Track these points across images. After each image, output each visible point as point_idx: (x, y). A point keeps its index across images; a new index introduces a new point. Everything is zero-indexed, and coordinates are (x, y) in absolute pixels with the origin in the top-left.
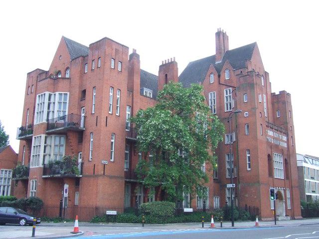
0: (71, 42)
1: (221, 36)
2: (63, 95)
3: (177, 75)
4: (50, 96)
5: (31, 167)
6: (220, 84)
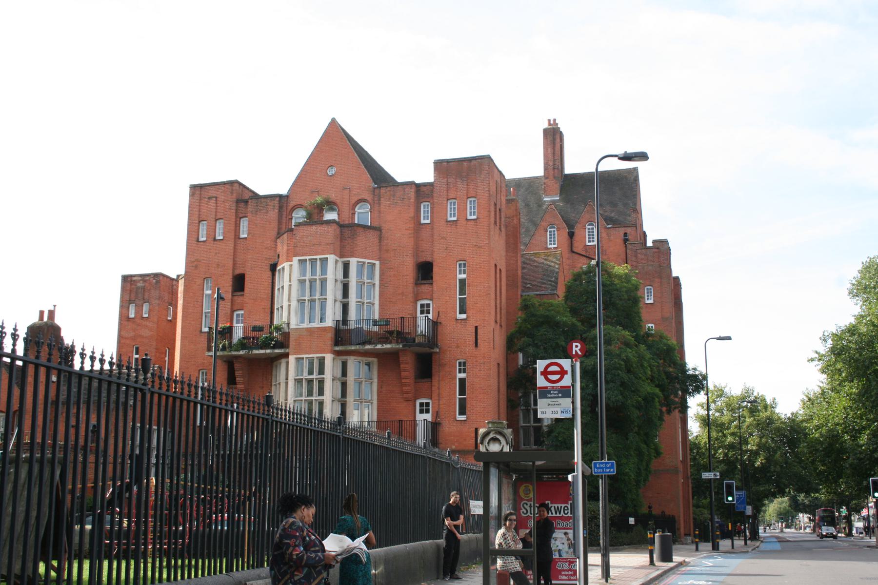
0: (637, 176)
1: (553, 137)
6: (379, 229)
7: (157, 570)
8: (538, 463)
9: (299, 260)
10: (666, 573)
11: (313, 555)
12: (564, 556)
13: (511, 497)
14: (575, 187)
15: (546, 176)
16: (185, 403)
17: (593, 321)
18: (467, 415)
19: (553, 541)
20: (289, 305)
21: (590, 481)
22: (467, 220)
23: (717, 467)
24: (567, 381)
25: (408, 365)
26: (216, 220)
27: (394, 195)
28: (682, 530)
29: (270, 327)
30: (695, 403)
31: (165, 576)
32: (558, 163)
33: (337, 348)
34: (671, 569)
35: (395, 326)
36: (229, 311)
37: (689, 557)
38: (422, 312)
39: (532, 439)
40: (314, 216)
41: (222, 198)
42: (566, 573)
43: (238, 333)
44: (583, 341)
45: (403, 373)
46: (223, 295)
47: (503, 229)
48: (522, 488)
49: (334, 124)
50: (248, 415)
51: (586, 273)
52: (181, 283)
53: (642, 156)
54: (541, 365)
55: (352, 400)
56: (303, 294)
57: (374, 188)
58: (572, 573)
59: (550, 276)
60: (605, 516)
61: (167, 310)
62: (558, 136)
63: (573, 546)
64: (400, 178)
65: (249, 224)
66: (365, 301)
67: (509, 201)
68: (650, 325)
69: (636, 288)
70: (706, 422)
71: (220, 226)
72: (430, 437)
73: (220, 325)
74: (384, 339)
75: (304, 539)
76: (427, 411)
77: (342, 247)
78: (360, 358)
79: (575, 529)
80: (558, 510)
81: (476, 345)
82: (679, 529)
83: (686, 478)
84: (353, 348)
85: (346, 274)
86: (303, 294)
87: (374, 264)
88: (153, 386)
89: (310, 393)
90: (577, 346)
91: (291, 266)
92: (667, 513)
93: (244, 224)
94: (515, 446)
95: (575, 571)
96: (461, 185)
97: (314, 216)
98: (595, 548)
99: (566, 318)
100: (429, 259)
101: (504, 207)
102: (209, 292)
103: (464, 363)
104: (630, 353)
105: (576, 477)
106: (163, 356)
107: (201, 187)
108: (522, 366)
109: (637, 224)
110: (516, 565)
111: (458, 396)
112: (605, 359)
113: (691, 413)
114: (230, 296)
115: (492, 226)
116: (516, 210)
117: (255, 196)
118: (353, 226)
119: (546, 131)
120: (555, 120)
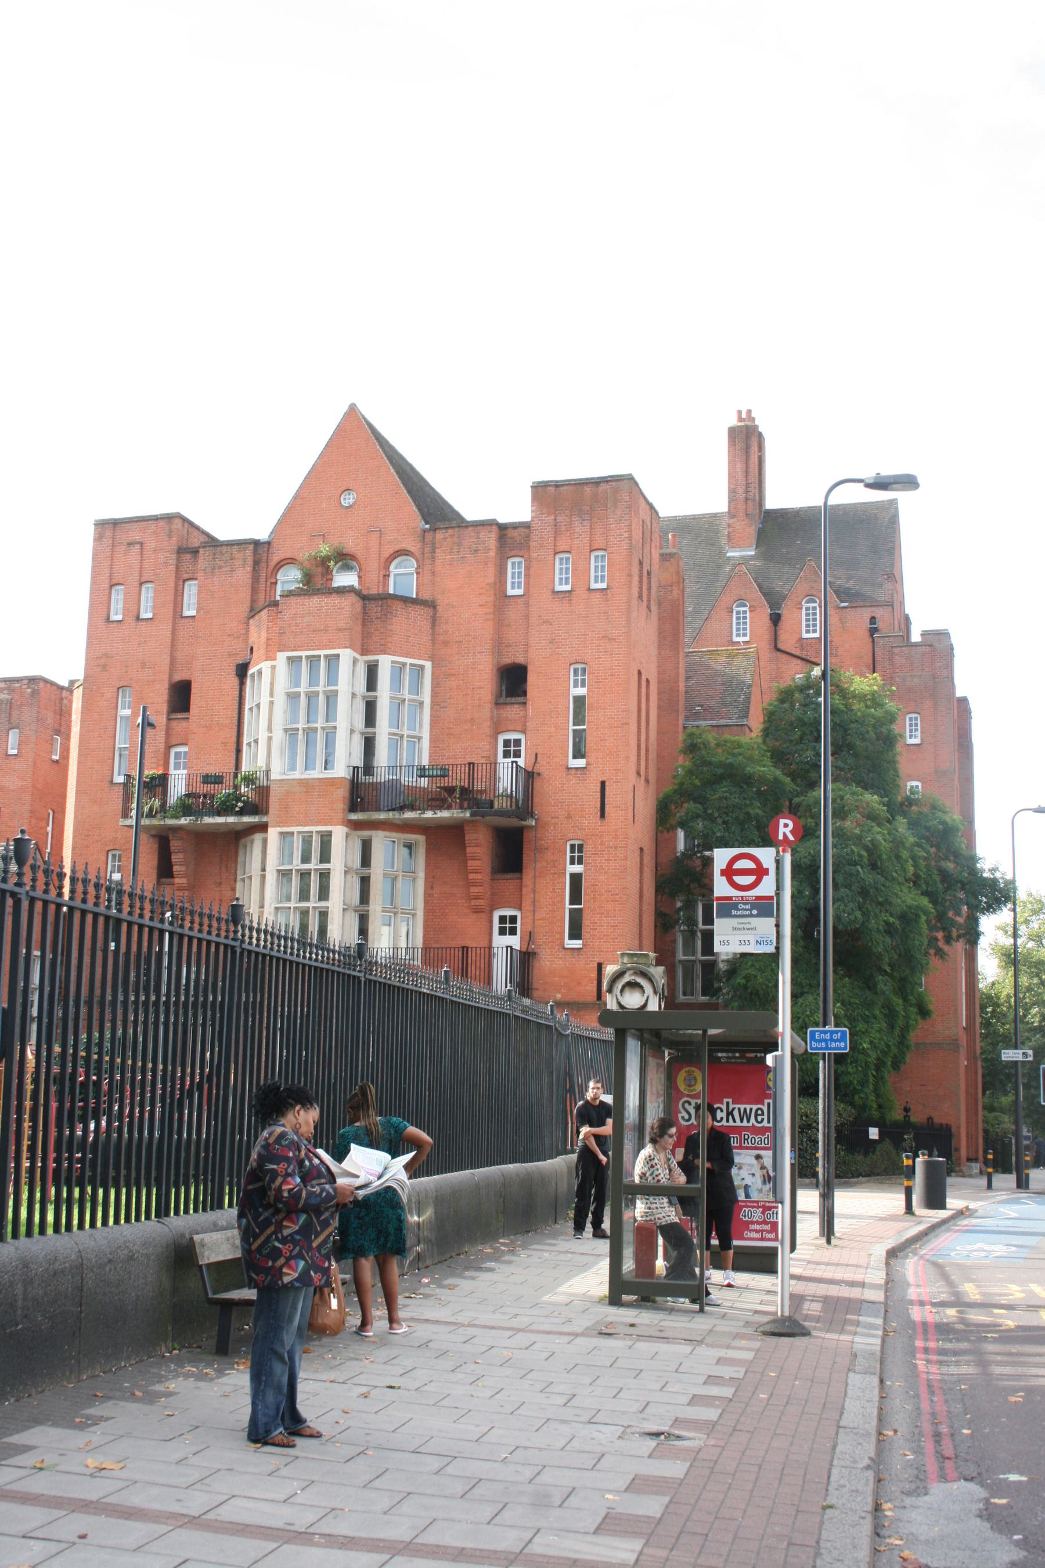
1: (746, 442)
2: (323, 663)
7: (37, 1206)
8: (712, 1032)
9: (289, 658)
10: (934, 1228)
11: (317, 1189)
12: (755, 1196)
13: (661, 1088)
14: (783, 533)
15: (732, 514)
16: (89, 918)
17: (813, 775)
18: (586, 943)
19: (734, 1171)
20: (270, 739)
21: (804, 1063)
22: (589, 590)
23: (1029, 1039)
24: (767, 887)
25: (480, 848)
26: (141, 584)
27: (459, 545)
28: (963, 1152)
29: (236, 776)
30: (993, 928)
31: (50, 1217)
32: (754, 491)
33: (354, 817)
34: (944, 1222)
35: (458, 779)
36: (162, 746)
37: (976, 1200)
38: (506, 755)
39: (699, 985)
40: (316, 580)
41: (151, 544)
42: (758, 1227)
43: (178, 787)
44: (794, 811)
45: (470, 863)
46: (152, 719)
47: (654, 607)
48: (682, 1075)
49: (353, 412)
50: (200, 940)
51: (802, 689)
52: (78, 695)
53: (909, 482)
54: (721, 856)
55: (379, 909)
56: (298, 720)
57: (425, 531)
58: (768, 1227)
59: (735, 694)
60: (827, 1125)
61: (51, 742)
62: (754, 442)
63: (771, 1179)
64: (470, 515)
65: (199, 592)
66: (406, 733)
67: (665, 557)
68: (914, 783)
69: (891, 718)
70: (1012, 959)
71: (147, 594)
72: (517, 977)
73: (146, 773)
74: (438, 801)
75: (301, 1163)
76: (513, 931)
77: (366, 636)
78: (395, 835)
79: (775, 1148)
80: (745, 1115)
81: (603, 815)
82: (958, 1150)
83: (971, 1057)
84: (382, 816)
85: (372, 683)
86: (298, 720)
87: (422, 667)
88: (33, 888)
89: (304, 895)
90: (786, 825)
91: (273, 668)
92: (937, 1120)
93: (191, 592)
94: (669, 1000)
95: (774, 1225)
96: (580, 528)
97: (316, 580)
98: (807, 1181)
99: (766, 769)
100: (520, 660)
101: (655, 567)
102: (127, 712)
103: (581, 847)
104: (879, 835)
105: (780, 1060)
106: (43, 824)
107: (115, 523)
108: (683, 854)
109: (894, 603)
110: (669, 1213)
111: (568, 906)
112: (834, 846)
113: (983, 943)
114: (164, 721)
115: (635, 602)
116: (678, 573)
117: (212, 542)
118: (386, 598)
119: (733, 432)
120: (749, 412)
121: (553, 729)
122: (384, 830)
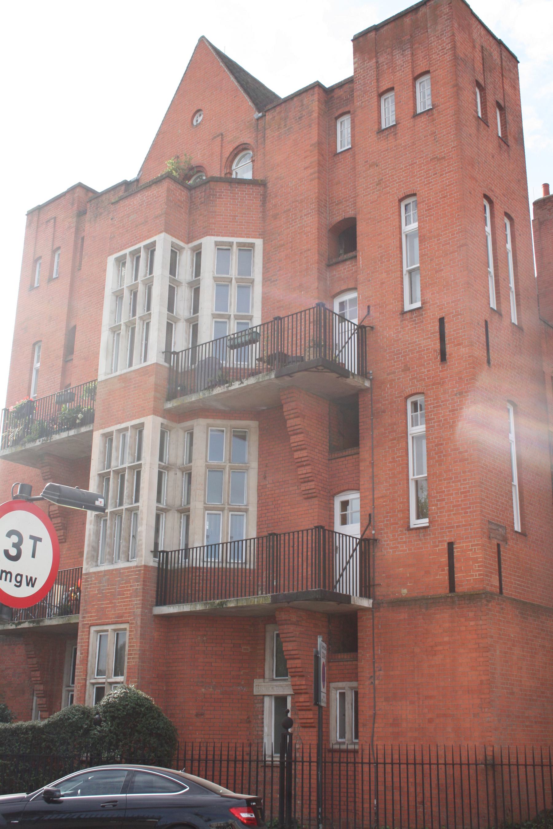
3: (397, 104)
4: (174, 254)
5: (87, 568)
25: (307, 425)
49: (203, 43)
87: (252, 245)
100: (350, 213)
107: (39, 209)
121: (384, 275)
122: (206, 417)
